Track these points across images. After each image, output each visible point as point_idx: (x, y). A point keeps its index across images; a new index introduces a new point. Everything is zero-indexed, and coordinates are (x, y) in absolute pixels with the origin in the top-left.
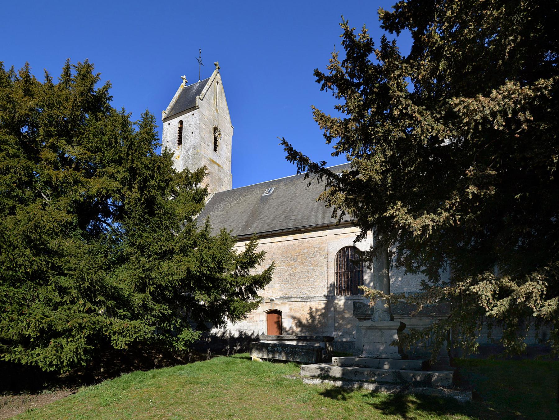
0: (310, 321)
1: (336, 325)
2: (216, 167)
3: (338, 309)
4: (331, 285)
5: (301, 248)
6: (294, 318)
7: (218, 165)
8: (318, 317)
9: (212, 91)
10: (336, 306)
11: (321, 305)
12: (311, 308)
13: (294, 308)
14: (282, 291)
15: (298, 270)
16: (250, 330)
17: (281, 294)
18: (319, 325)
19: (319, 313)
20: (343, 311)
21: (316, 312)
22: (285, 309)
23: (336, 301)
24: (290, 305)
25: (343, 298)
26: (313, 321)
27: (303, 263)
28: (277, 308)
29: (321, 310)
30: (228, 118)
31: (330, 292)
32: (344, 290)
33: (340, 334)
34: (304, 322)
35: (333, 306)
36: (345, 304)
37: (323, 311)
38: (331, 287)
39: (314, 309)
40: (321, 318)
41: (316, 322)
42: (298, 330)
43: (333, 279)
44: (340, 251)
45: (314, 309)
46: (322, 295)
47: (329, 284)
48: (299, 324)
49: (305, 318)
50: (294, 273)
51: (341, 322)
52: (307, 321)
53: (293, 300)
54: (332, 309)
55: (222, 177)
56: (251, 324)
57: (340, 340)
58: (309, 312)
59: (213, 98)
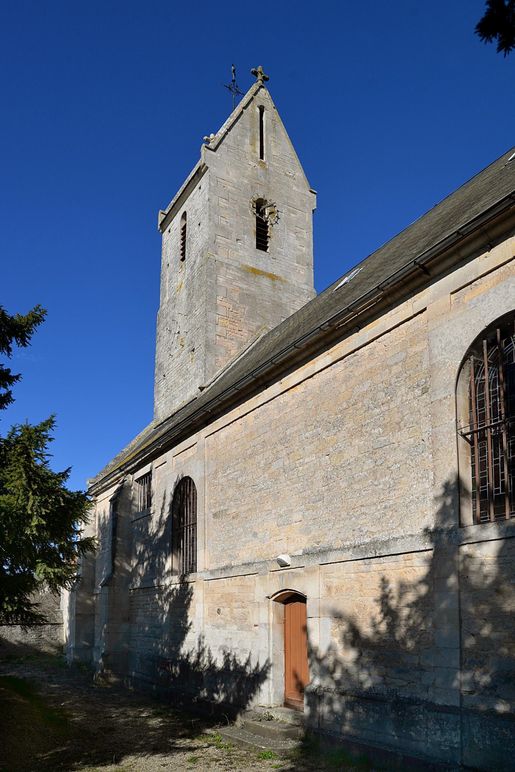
0: (383, 627)
1: (470, 642)
2: (266, 282)
3: (474, 579)
4: (446, 486)
5: (352, 382)
6: (338, 616)
7: (272, 277)
8: (405, 612)
9: (244, 128)
10: (466, 569)
11: (416, 568)
12: (384, 582)
13: (335, 582)
14: (307, 531)
15: (346, 456)
16: (244, 650)
17: (304, 543)
18: (410, 644)
19: (410, 597)
20: (496, 588)
21: (401, 595)
22: (311, 587)
23: (465, 549)
24: (326, 575)
25: (492, 531)
26: (392, 627)
27: (359, 431)
28: (297, 586)
29: (414, 586)
30: (299, 174)
31: (443, 514)
32: (499, 501)
33: (485, 679)
34: (366, 630)
35: (453, 570)
36: (502, 557)
37: (423, 590)
38: (445, 494)
39: (393, 586)
40: (417, 618)
41: (401, 632)
42: (349, 656)
43: (454, 461)
44: (475, 347)
45: (393, 586)
46: (418, 530)
47: (440, 484)
48: (354, 637)
49: (369, 618)
50: (336, 468)
51: (486, 631)
52: (374, 625)
53: (332, 557)
54: (452, 580)
55: (284, 300)
56: (245, 633)
57: (483, 707)
58: (378, 594)
59: (247, 141)
